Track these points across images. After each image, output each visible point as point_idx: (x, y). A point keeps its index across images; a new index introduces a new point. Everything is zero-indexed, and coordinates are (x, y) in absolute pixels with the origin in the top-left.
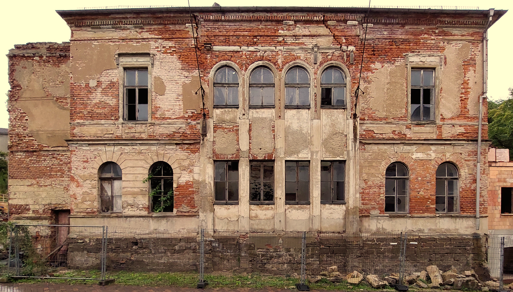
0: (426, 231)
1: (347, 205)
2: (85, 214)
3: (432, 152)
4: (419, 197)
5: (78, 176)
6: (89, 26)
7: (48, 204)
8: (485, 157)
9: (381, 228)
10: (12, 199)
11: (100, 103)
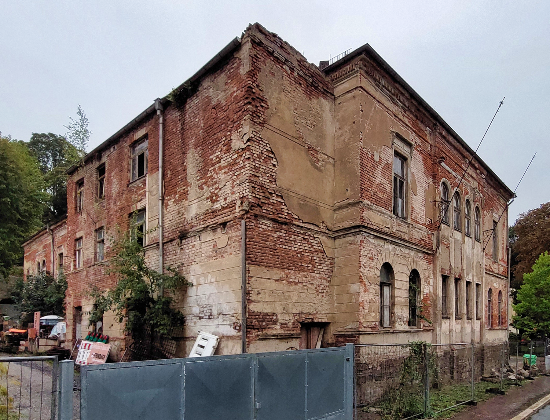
1: (482, 320)
5: (365, 277)
6: (375, 80)
7: (299, 314)
10: (254, 302)
11: (380, 185)
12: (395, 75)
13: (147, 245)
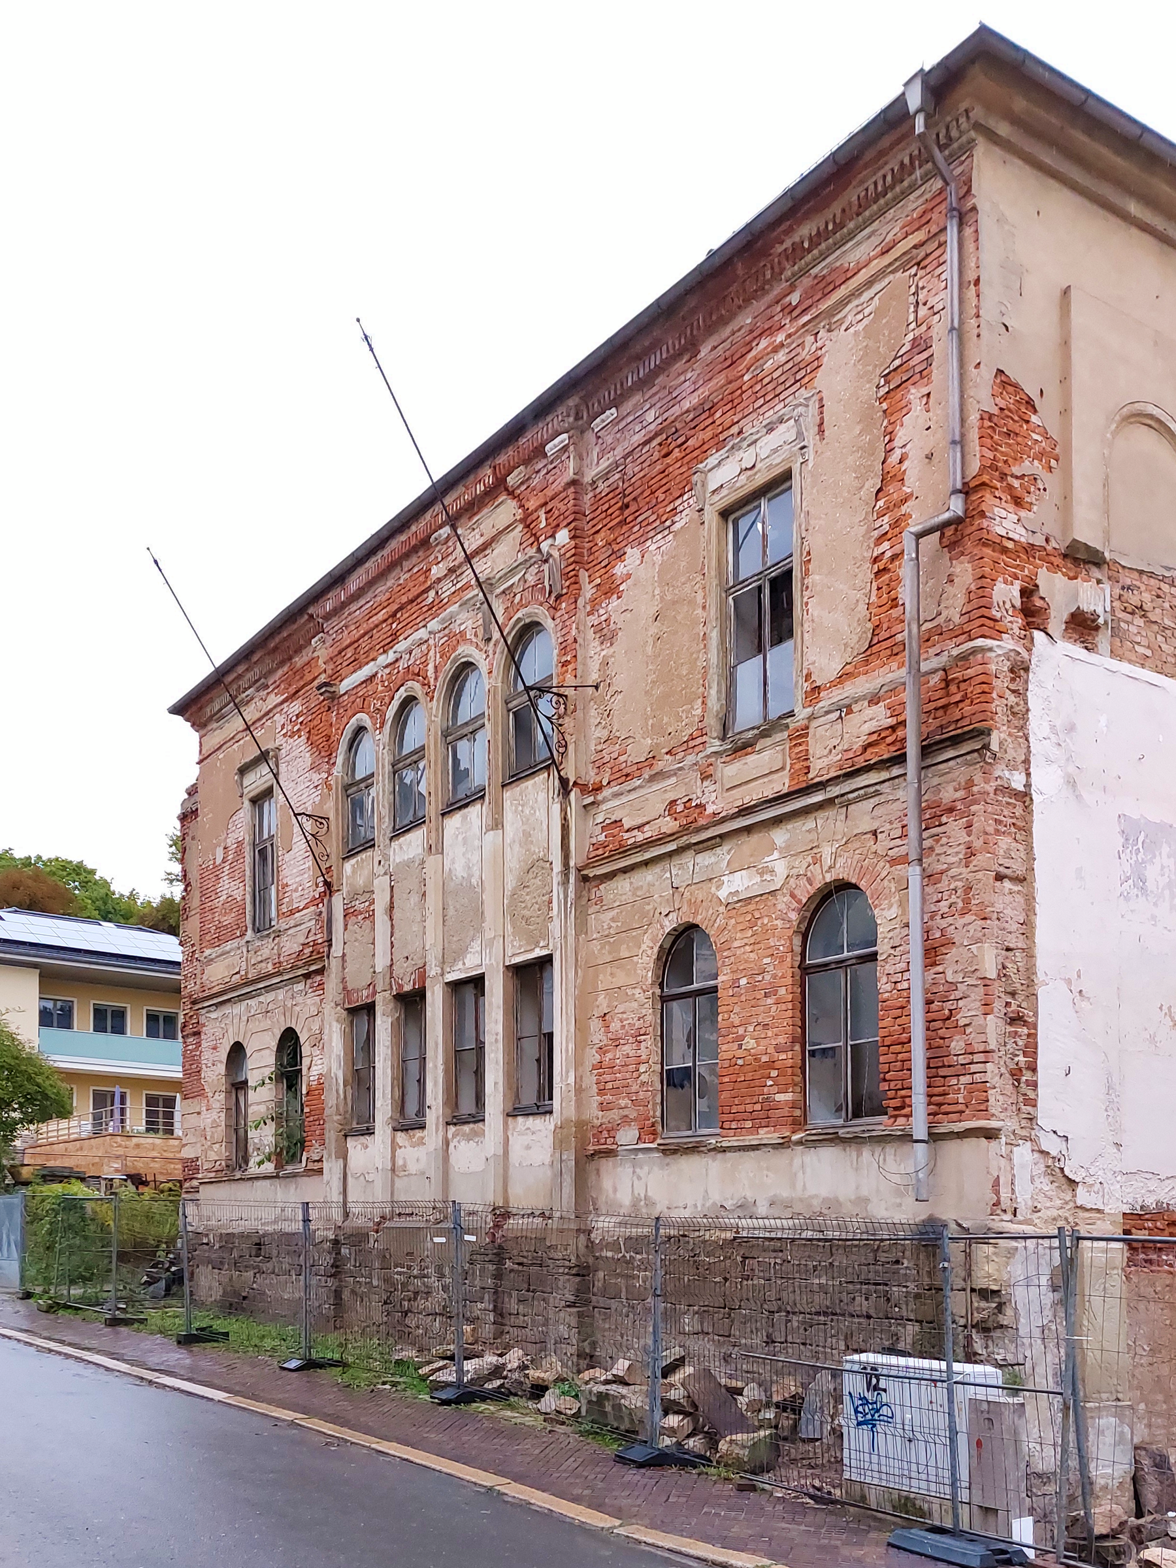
0: (762, 1210)
2: (213, 1175)
3: (776, 855)
4: (740, 1062)
8: (969, 826)
9: (642, 1196)
12: (947, 68)
13: (731, 584)
